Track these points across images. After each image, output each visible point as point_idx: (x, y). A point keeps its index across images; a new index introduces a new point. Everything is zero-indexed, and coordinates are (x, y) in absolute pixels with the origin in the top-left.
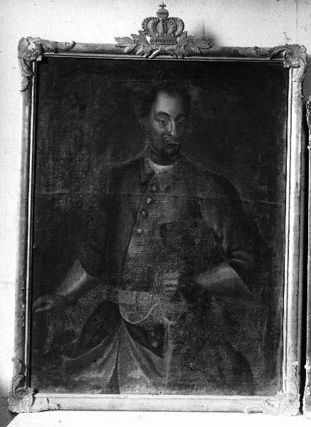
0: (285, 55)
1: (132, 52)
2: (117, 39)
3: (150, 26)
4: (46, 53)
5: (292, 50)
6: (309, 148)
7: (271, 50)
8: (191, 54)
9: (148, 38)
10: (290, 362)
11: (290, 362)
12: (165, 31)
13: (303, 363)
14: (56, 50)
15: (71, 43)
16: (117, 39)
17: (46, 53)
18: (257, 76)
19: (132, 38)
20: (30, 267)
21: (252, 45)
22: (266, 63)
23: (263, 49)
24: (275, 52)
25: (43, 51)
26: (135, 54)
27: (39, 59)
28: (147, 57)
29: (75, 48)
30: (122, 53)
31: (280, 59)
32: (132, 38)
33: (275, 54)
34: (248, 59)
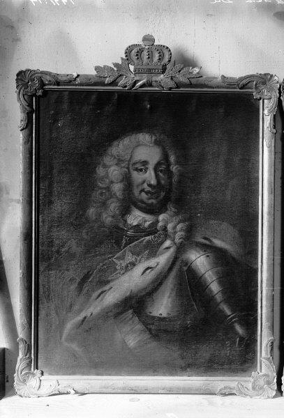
0: (256, 84)
1: (114, 83)
2: (97, 68)
3: (134, 52)
4: (46, 87)
5: (265, 79)
6: (282, 98)
7: (241, 79)
8: (178, 85)
9: (132, 68)
10: (265, 338)
11: (265, 338)
12: (150, 57)
13: (280, 96)
14: (58, 83)
15: (75, 75)
16: (97, 68)
17: (46, 87)
18: (235, 103)
19: (115, 69)
20: (35, 297)
21: (20, 137)
22: (234, 94)
23: (230, 78)
24: (244, 82)
25: (42, 84)
26: (117, 86)
27: (40, 93)
28: (131, 89)
29: (78, 81)
30: (103, 84)
31: (250, 90)
32: (115, 69)
33: (246, 83)
34: (215, 90)
